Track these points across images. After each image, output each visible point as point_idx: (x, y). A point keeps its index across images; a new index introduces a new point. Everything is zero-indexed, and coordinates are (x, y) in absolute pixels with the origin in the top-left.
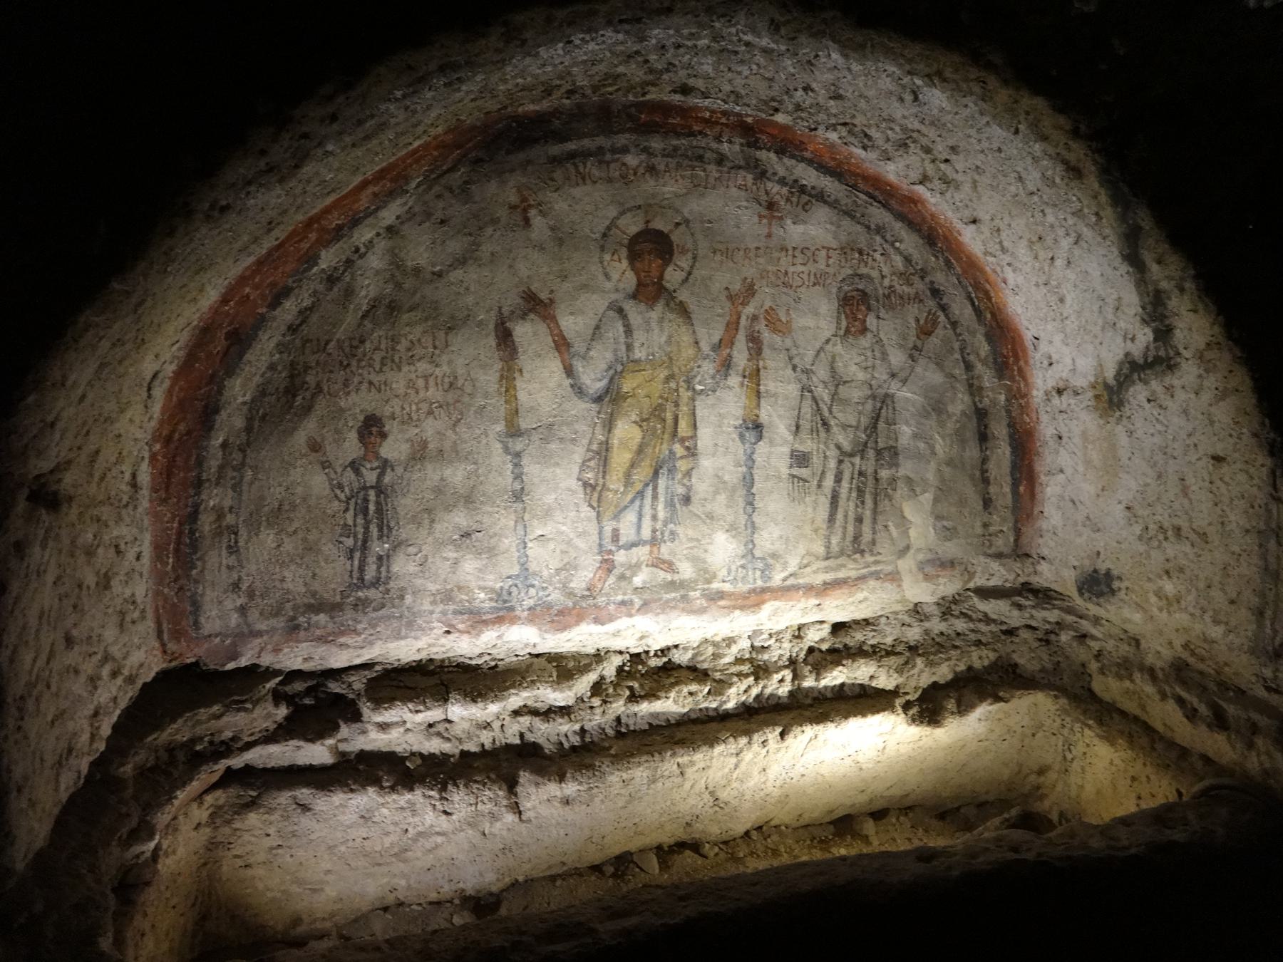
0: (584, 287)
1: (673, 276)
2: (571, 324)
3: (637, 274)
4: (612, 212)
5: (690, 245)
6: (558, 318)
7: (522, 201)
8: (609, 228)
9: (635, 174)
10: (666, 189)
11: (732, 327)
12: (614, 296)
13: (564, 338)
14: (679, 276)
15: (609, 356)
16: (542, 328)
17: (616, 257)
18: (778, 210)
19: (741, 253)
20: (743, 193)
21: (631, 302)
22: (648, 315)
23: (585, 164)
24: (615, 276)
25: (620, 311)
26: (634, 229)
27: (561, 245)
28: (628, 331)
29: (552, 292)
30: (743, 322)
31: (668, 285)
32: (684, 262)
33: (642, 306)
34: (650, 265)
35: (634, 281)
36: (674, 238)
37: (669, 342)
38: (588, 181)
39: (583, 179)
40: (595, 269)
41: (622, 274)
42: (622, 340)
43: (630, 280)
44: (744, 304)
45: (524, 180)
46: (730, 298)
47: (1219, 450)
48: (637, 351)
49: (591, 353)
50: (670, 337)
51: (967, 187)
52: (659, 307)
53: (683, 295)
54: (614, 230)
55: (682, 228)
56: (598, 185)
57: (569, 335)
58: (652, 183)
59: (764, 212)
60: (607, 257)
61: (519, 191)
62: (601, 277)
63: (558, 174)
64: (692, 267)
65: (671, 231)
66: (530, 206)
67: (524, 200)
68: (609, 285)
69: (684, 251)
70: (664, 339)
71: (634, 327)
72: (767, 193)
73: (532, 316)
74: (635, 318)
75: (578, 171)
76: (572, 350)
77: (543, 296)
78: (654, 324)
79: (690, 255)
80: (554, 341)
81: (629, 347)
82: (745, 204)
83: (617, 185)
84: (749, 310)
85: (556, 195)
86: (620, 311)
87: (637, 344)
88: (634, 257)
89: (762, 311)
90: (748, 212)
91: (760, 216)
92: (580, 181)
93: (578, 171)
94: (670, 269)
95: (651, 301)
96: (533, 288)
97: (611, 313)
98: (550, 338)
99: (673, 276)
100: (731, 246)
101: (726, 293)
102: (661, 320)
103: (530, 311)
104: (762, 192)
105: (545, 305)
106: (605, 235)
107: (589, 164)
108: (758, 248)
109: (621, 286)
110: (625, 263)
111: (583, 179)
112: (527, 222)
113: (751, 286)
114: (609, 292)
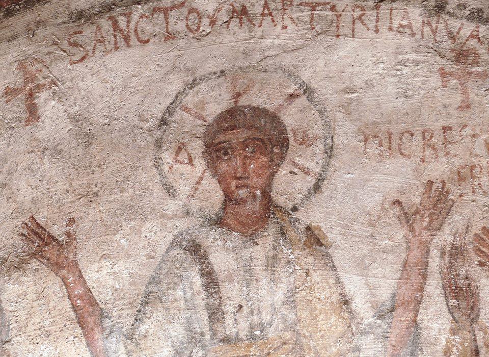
0: (131, 211)
1: (288, 185)
2: (104, 276)
3: (222, 180)
4: (175, 85)
5: (317, 130)
6: (82, 265)
7: (26, 82)
8: (170, 111)
9: (213, 23)
10: (268, 42)
11: (415, 271)
12: (182, 224)
13: (92, 302)
14: (303, 184)
15: (177, 332)
16: (54, 285)
17: (183, 157)
18: (476, 63)
19: (418, 139)
20: (406, 40)
21: (215, 233)
22: (246, 253)
23: (128, 16)
24: (184, 189)
25: (196, 250)
26: (214, 110)
27: (88, 144)
28: (211, 281)
29: (72, 221)
30: (435, 262)
31: (280, 200)
32: (310, 159)
33: (236, 238)
34: (245, 167)
35: (218, 196)
36: (290, 119)
37: (290, 301)
38: (133, 40)
39: (127, 39)
40: (147, 177)
41: (195, 184)
42: (200, 301)
43: (212, 194)
44: (435, 228)
45: (31, 49)
46: (407, 217)
47: (85, 66)
48: (229, 321)
49: (143, 328)
50: (292, 292)
51: (256, 33)
52: (268, 238)
53: (313, 215)
54: (179, 114)
55: (303, 101)
56: (150, 46)
57: (102, 296)
58: (242, 34)
59: (450, 67)
60: (167, 157)
61: (22, 65)
62: (158, 192)
63: (88, 32)
64: (325, 168)
65: (280, 107)
66: (39, 87)
67: (29, 78)
68: (172, 206)
69: (306, 141)
70: (279, 296)
71: (221, 276)
72: (452, 37)
73: (34, 264)
74: (221, 259)
75: (115, 25)
76: (107, 323)
77: (57, 230)
78: (259, 269)
79: (319, 147)
80: (75, 308)
81: (215, 314)
82: (413, 56)
83: (182, 43)
84: (445, 238)
85: (80, 68)
86: (196, 250)
87: (229, 308)
88: (215, 151)
89: (470, 237)
90: (423, 69)
91: (443, 74)
92: (121, 43)
93: (115, 25)
94: (283, 172)
95: (250, 229)
96: (40, 219)
97: (178, 252)
98: (67, 303)
99: (288, 185)
100: (396, 129)
101: (397, 210)
102: (272, 263)
103: (33, 255)
104: (442, 35)
105: (60, 245)
106: (163, 122)
107: (135, 16)
108: (446, 129)
109: (195, 205)
110: (200, 165)
111: (127, 39)
112: (33, 112)
113: (444, 194)
114: (174, 217)
